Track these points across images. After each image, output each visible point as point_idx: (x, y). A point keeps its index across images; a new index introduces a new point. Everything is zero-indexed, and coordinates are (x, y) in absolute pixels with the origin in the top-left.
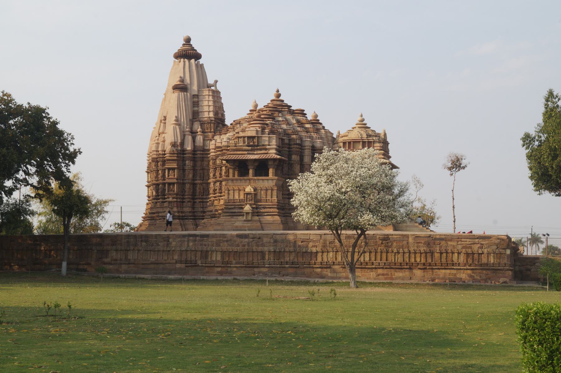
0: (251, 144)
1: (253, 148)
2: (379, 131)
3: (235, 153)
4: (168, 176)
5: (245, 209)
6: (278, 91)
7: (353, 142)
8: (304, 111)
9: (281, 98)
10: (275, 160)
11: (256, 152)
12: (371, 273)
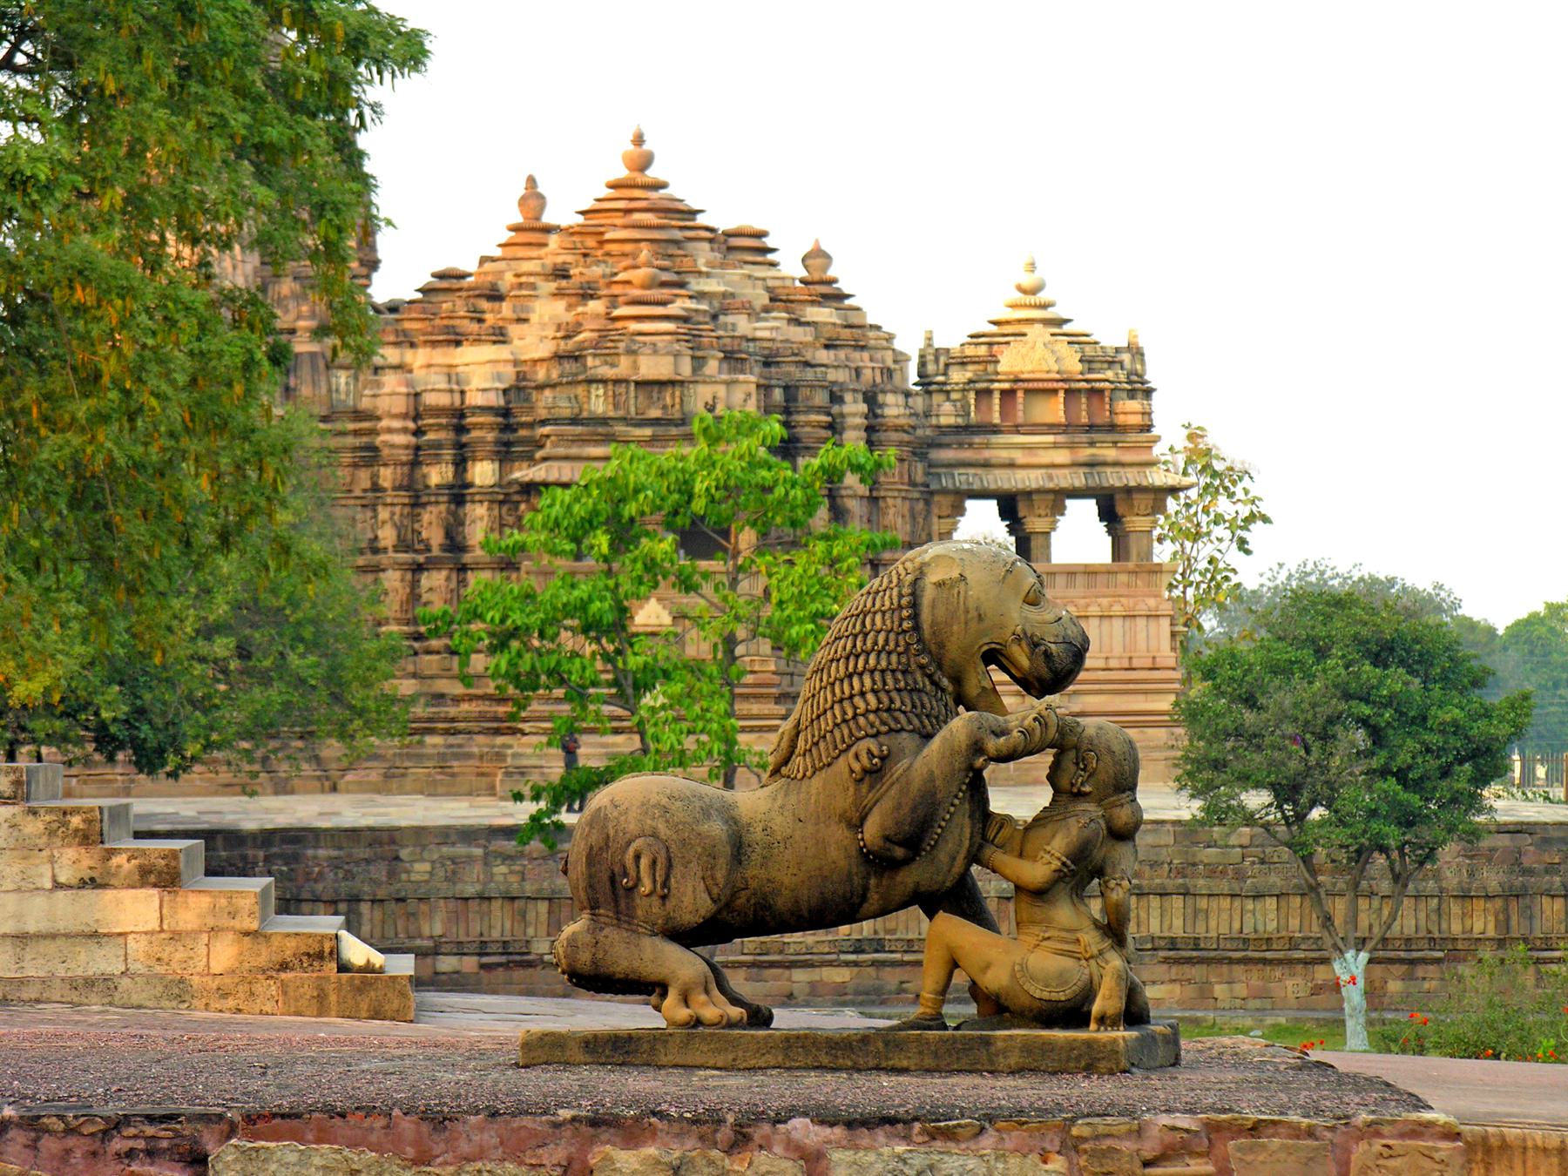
0: (655, 413)
1: (660, 430)
3: (574, 451)
6: (639, 140)
7: (1027, 391)
8: (761, 235)
9: (653, 173)
12: (1289, 983)
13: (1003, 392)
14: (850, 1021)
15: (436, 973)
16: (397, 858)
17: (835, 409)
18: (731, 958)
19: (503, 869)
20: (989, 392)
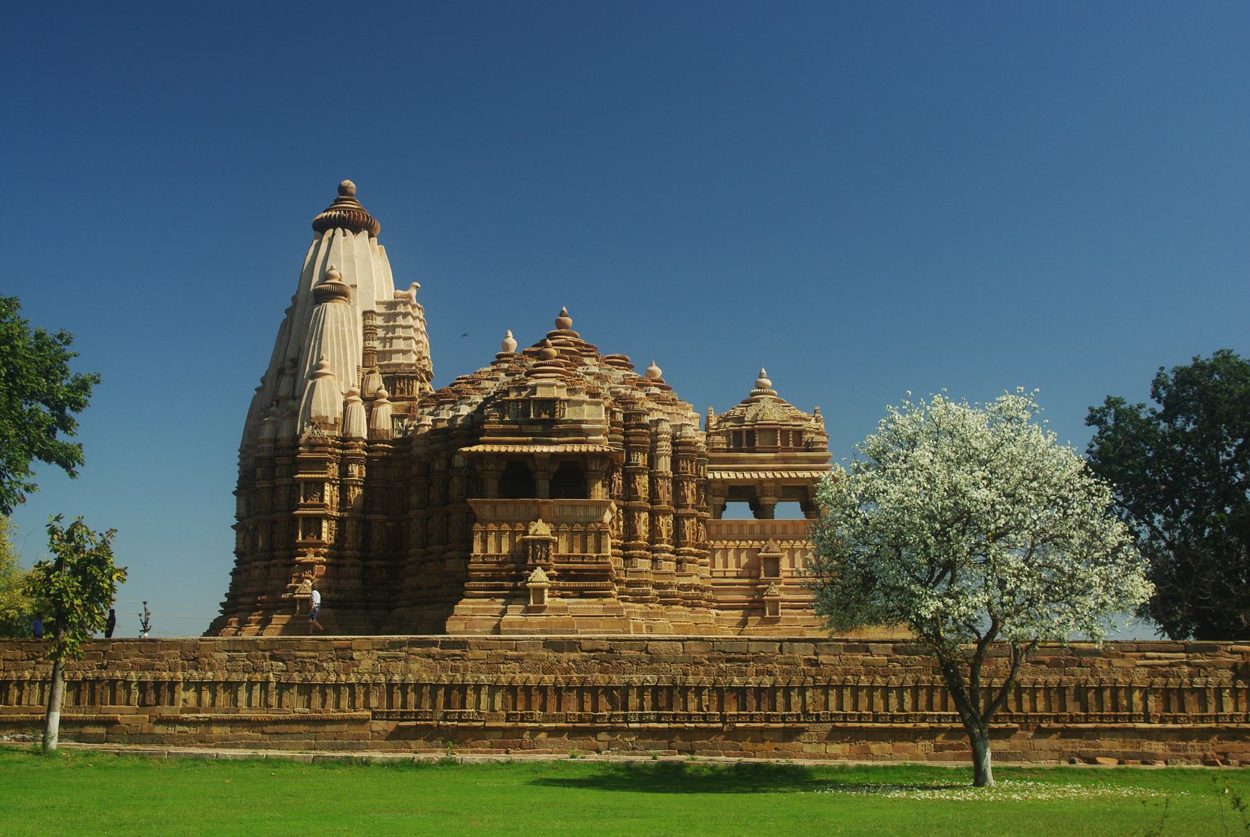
7: (760, 430)
10: (602, 456)
13: (747, 431)
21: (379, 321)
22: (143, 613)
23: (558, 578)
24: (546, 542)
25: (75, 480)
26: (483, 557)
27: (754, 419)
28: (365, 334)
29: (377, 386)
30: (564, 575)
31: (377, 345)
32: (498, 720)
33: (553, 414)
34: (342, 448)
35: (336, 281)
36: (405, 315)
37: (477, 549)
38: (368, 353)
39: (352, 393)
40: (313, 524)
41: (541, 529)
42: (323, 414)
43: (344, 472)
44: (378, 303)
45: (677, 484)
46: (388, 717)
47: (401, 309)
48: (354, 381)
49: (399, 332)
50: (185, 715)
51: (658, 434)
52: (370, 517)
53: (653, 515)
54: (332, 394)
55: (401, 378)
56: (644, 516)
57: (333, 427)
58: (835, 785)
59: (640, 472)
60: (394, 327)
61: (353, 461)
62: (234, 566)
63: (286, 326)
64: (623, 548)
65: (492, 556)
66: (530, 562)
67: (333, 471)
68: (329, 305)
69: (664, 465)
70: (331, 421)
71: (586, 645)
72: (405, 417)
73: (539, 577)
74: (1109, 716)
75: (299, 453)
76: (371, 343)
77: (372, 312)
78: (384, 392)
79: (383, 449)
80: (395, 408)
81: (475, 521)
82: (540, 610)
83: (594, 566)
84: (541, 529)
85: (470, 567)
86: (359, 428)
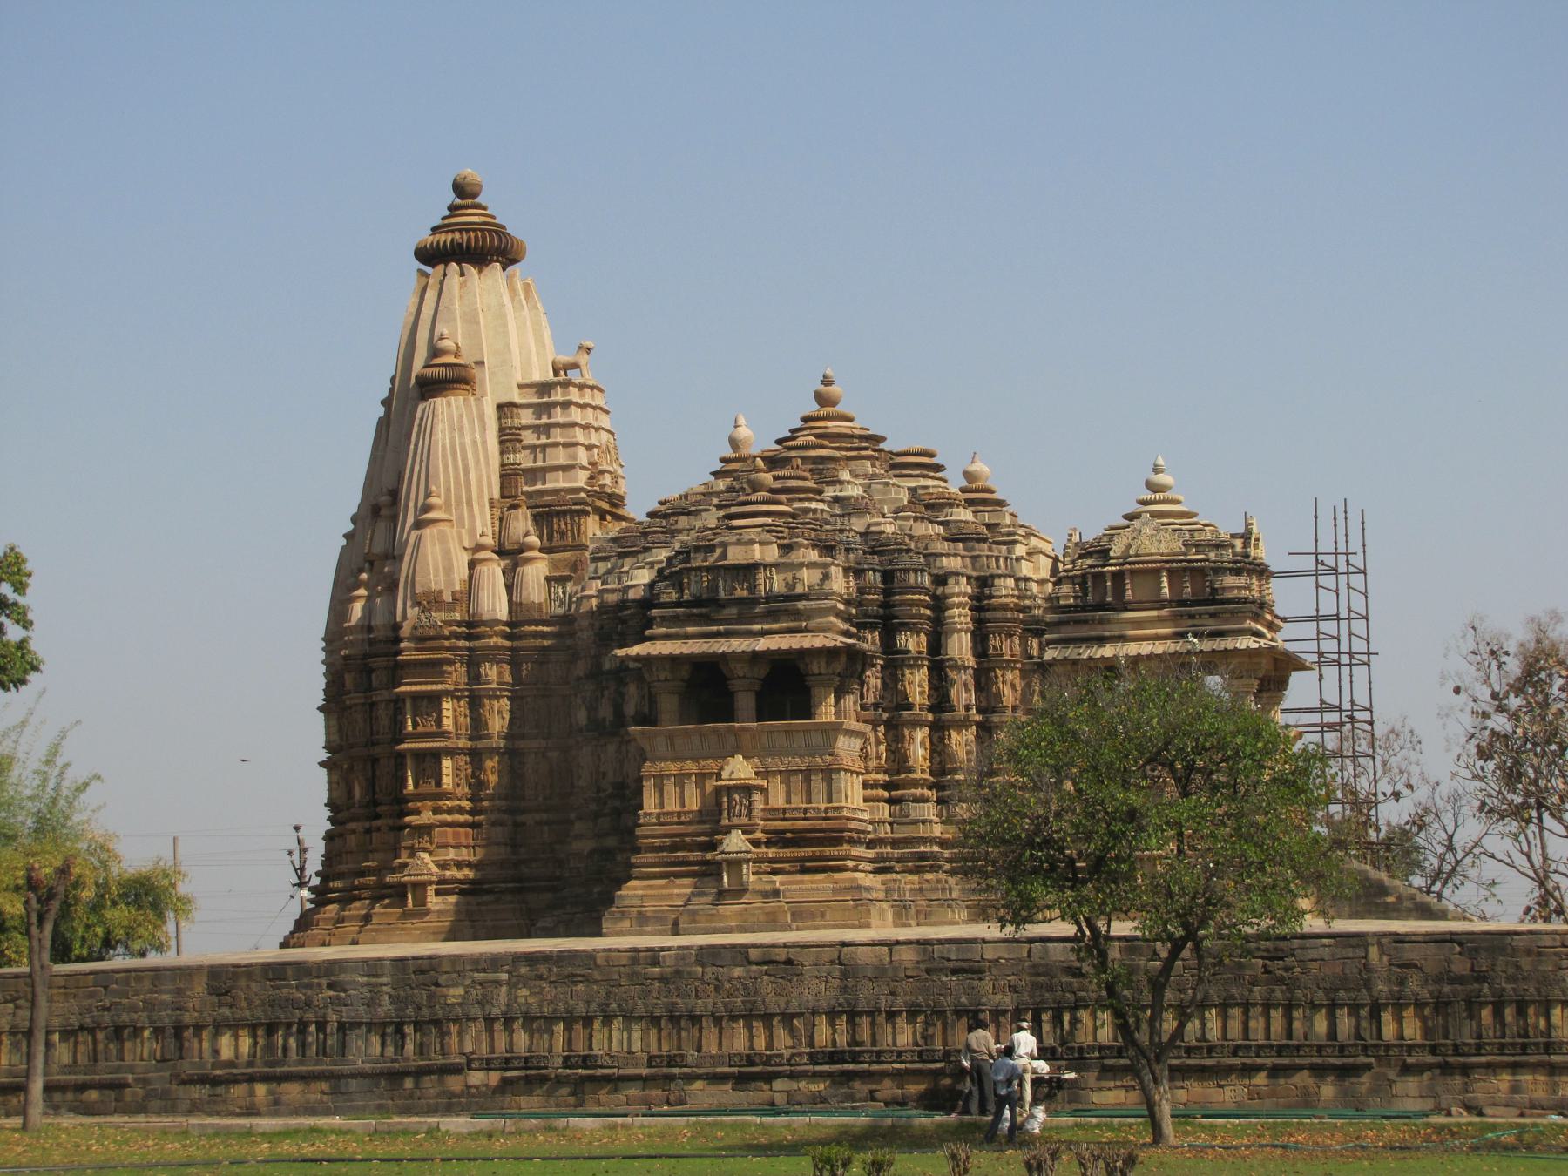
2: (1228, 526)
4: (415, 725)
5: (720, 848)
7: (1132, 572)
10: (831, 653)
11: (757, 627)
13: (1114, 574)
14: (527, 628)
15: (469, 1087)
16: (437, 985)
17: (940, 591)
18: (719, 1070)
19: (525, 992)
20: (1103, 574)
21: (527, 418)
22: (294, 846)
23: (768, 844)
24: (747, 790)
25: (470, 172)
26: (659, 815)
27: (1125, 555)
28: (501, 442)
29: (522, 531)
30: (777, 839)
31: (524, 460)
32: (636, 1066)
33: (753, 588)
34: (469, 637)
35: (450, 359)
36: (566, 405)
37: (650, 803)
38: (509, 475)
39: (479, 548)
40: (428, 762)
41: (740, 769)
42: (433, 587)
43: (475, 678)
44: (521, 386)
45: (984, 678)
46: (488, 1065)
47: (558, 395)
48: (484, 525)
49: (557, 436)
50: (218, 1072)
51: (947, 597)
52: (521, 744)
53: (938, 730)
54: (447, 555)
55: (561, 514)
56: (921, 734)
57: (451, 607)
58: (730, 1148)
59: (915, 663)
60: (548, 427)
61: (486, 658)
62: (329, 826)
63: (384, 425)
64: (887, 786)
65: (671, 814)
66: (725, 822)
67: (457, 675)
68: (438, 400)
69: (960, 646)
70: (447, 597)
71: (754, 954)
72: (569, 578)
73: (735, 842)
74: (1513, 1045)
75: (399, 652)
76: (511, 458)
77: (512, 405)
78: (533, 539)
79: (536, 635)
80: (554, 565)
81: (645, 760)
82: (740, 891)
83: (824, 824)
84: (740, 769)
85: (638, 831)
86: (494, 603)
